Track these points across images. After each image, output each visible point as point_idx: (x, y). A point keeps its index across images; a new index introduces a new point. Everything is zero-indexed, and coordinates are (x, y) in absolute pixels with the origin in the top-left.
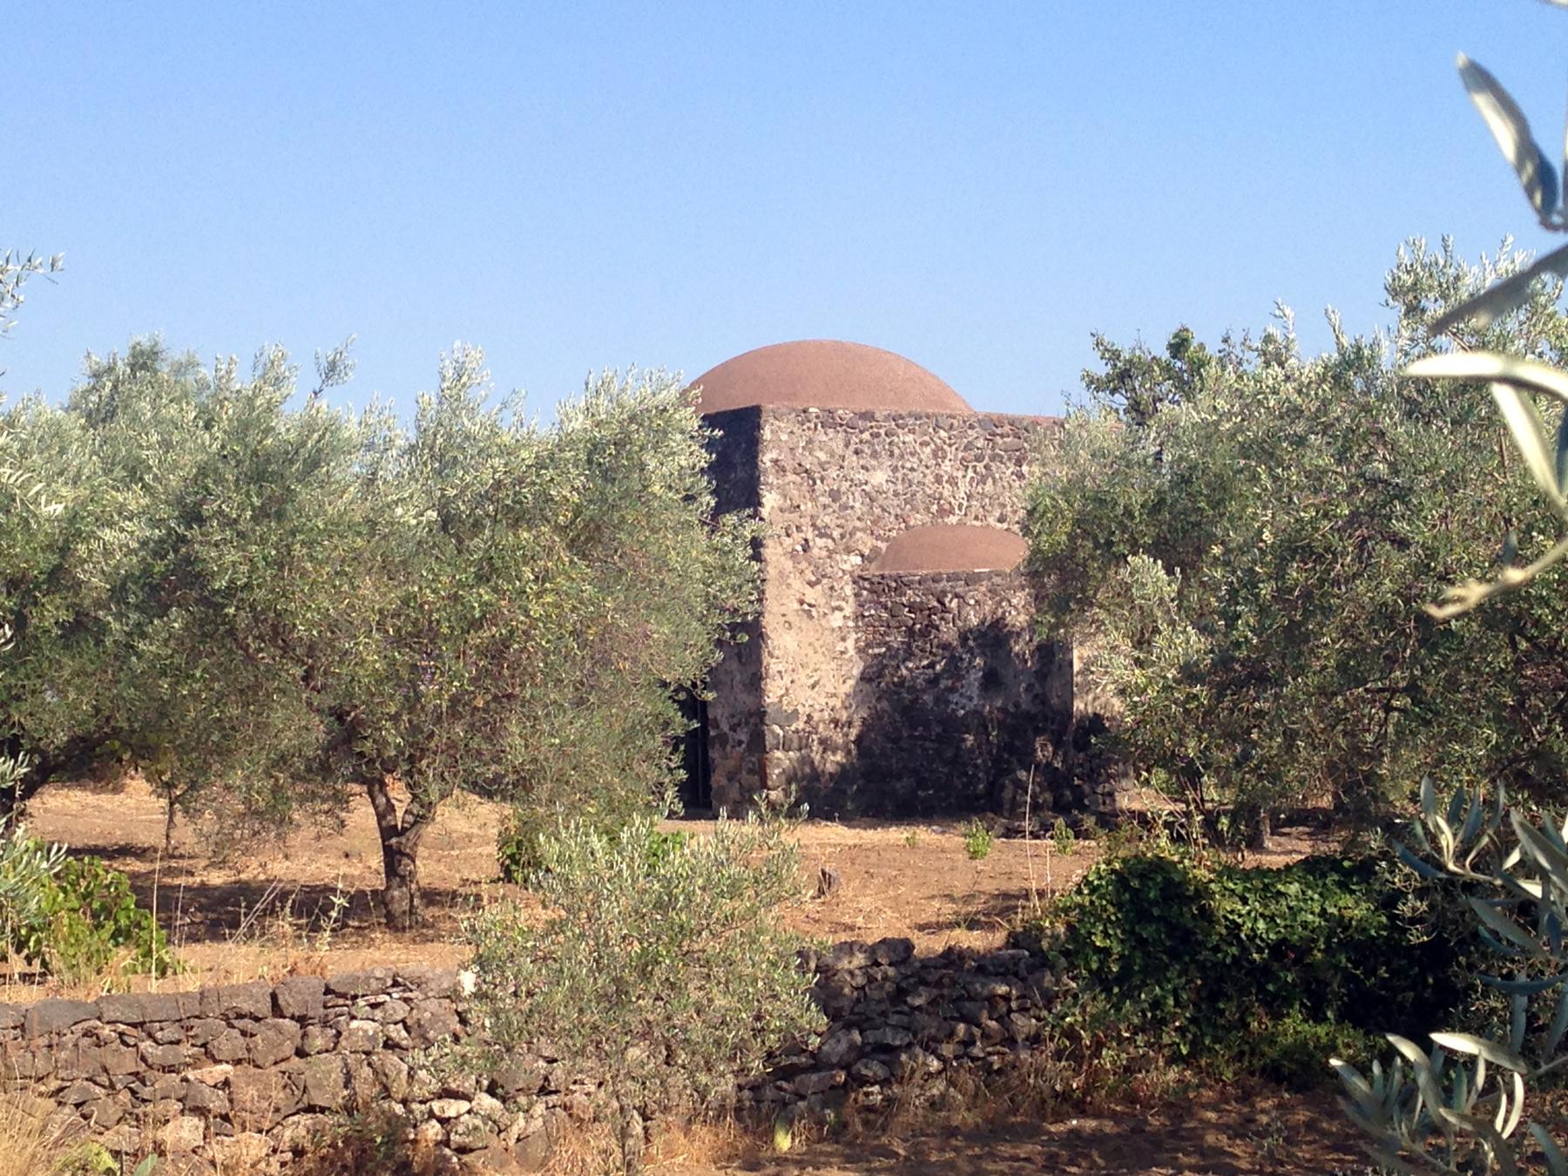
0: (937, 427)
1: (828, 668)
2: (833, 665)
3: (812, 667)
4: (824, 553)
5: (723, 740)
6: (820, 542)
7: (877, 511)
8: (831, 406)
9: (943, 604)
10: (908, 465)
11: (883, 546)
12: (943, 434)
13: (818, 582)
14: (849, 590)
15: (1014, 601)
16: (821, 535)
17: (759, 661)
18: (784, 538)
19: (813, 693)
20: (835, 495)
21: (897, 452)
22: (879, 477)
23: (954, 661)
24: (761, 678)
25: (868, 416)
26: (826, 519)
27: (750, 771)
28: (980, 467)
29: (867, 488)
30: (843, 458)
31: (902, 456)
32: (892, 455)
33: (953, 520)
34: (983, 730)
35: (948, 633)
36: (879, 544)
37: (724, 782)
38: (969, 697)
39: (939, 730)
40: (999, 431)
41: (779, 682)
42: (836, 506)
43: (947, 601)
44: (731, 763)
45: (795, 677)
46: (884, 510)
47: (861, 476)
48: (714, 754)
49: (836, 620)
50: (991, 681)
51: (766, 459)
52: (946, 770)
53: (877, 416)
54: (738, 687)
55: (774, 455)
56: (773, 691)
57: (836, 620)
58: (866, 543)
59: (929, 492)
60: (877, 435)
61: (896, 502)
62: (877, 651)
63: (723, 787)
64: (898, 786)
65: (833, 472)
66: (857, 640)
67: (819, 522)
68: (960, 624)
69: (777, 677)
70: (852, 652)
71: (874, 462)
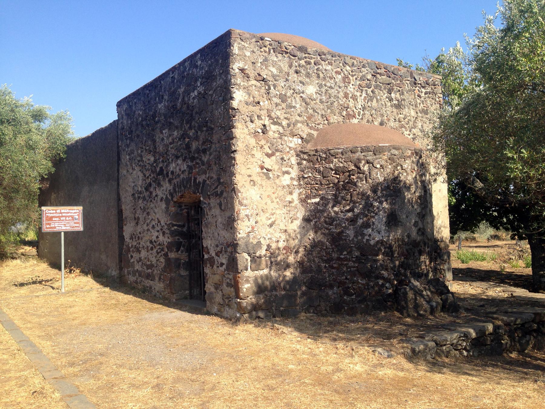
0: (345, 63)
1: (281, 212)
2: (285, 211)
3: (270, 211)
4: (276, 135)
5: (211, 261)
6: (274, 128)
7: (311, 111)
8: (279, 38)
9: (359, 168)
10: (328, 84)
11: (315, 133)
12: (348, 68)
13: (273, 154)
14: (294, 160)
15: (405, 166)
16: (275, 123)
17: (233, 208)
18: (249, 123)
19: (271, 230)
20: (283, 98)
21: (321, 75)
22: (311, 90)
23: (368, 206)
24: (234, 220)
25: (303, 49)
26: (278, 113)
27: (228, 285)
28: (369, 91)
29: (304, 96)
30: (288, 74)
31: (324, 78)
32: (318, 77)
33: (355, 121)
34: (389, 252)
35: (364, 186)
36: (312, 132)
37: (213, 290)
38: (378, 233)
39: (357, 253)
40: (379, 71)
41: (247, 223)
42: (284, 105)
43: (361, 165)
44: (217, 278)
45: (258, 218)
46: (314, 111)
47: (299, 87)
48: (207, 270)
49: (286, 180)
50: (393, 220)
51: (236, 66)
52: (364, 282)
53: (309, 50)
54: (220, 225)
55: (241, 65)
56: (243, 229)
57: (286, 180)
58: (304, 131)
59: (341, 103)
60: (309, 63)
61: (322, 107)
62: (313, 201)
63: (211, 293)
64: (330, 293)
65: (281, 83)
66: (300, 194)
67: (273, 115)
68: (370, 181)
69: (246, 219)
70: (296, 202)
71: (308, 80)
